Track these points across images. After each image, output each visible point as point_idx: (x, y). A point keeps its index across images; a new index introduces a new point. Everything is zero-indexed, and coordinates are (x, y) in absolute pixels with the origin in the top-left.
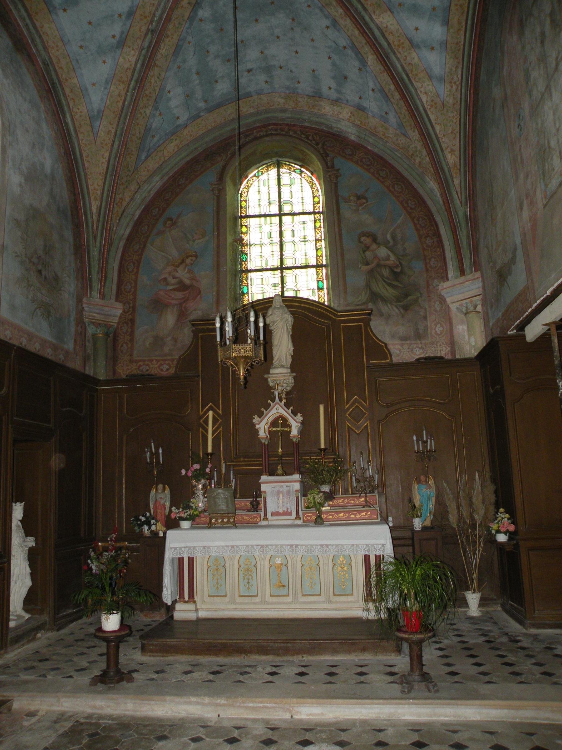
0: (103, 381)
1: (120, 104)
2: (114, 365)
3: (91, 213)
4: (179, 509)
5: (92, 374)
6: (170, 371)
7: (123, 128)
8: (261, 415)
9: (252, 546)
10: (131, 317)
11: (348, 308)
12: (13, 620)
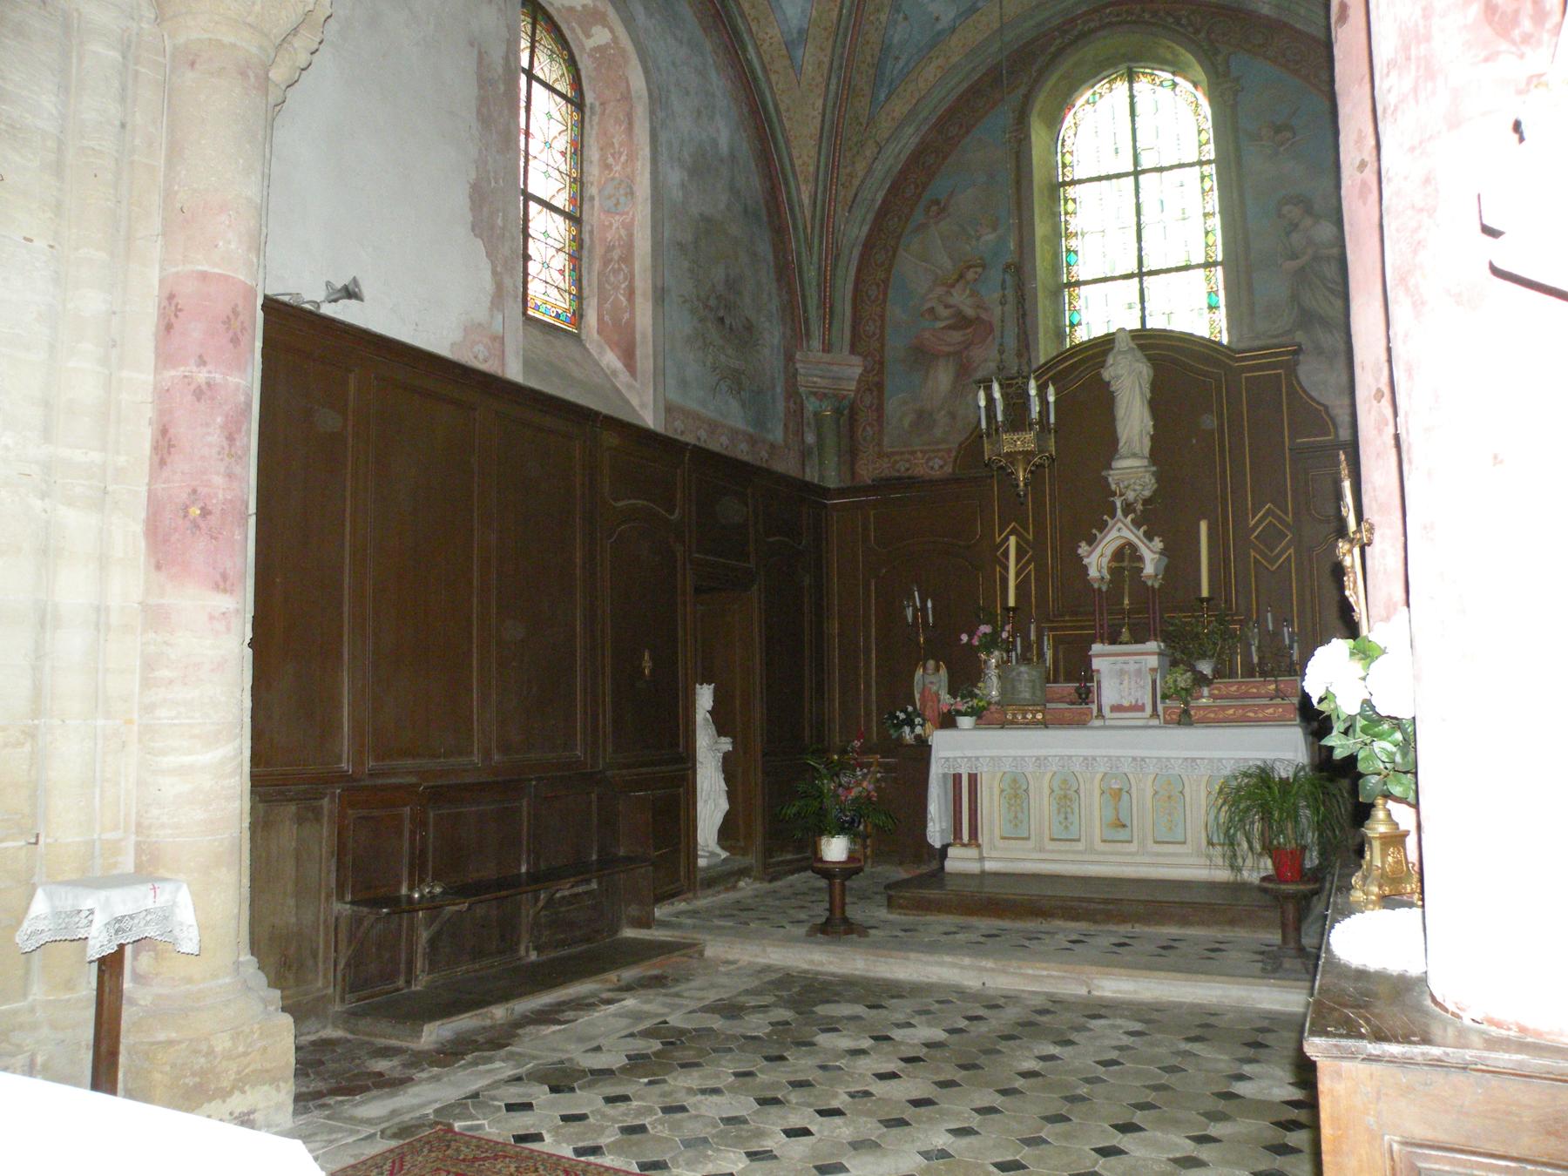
0: (834, 490)
1: (835, 14)
2: (853, 464)
3: (801, 206)
4: (955, 698)
5: (816, 481)
6: (945, 468)
7: (843, 53)
8: (1091, 541)
9: (1070, 757)
10: (876, 379)
11: (1257, 343)
12: (702, 857)
